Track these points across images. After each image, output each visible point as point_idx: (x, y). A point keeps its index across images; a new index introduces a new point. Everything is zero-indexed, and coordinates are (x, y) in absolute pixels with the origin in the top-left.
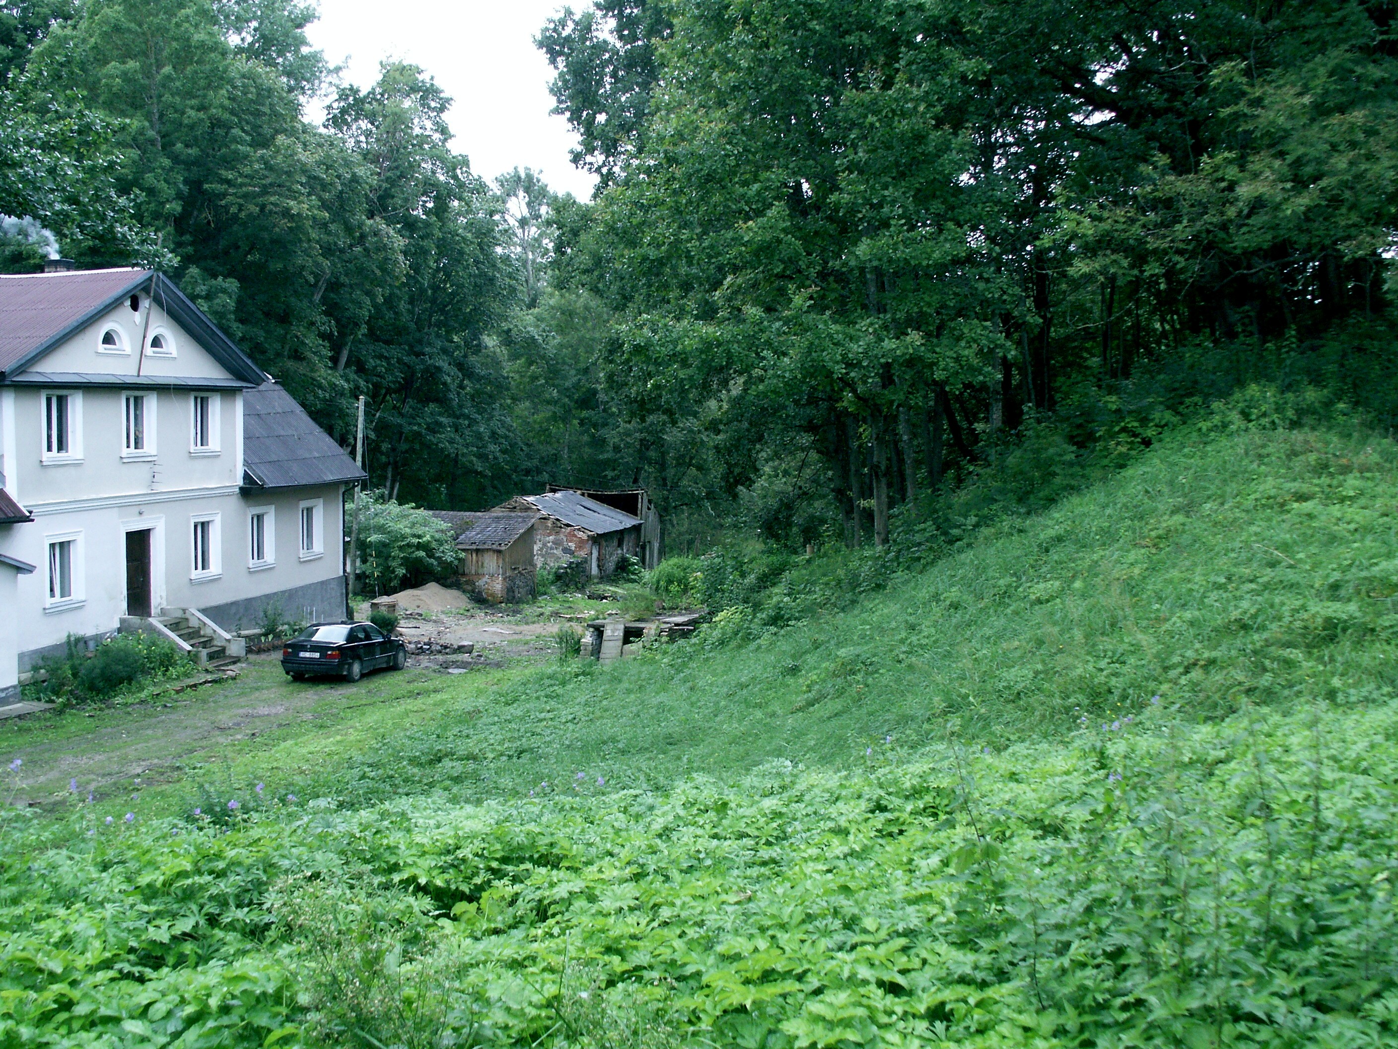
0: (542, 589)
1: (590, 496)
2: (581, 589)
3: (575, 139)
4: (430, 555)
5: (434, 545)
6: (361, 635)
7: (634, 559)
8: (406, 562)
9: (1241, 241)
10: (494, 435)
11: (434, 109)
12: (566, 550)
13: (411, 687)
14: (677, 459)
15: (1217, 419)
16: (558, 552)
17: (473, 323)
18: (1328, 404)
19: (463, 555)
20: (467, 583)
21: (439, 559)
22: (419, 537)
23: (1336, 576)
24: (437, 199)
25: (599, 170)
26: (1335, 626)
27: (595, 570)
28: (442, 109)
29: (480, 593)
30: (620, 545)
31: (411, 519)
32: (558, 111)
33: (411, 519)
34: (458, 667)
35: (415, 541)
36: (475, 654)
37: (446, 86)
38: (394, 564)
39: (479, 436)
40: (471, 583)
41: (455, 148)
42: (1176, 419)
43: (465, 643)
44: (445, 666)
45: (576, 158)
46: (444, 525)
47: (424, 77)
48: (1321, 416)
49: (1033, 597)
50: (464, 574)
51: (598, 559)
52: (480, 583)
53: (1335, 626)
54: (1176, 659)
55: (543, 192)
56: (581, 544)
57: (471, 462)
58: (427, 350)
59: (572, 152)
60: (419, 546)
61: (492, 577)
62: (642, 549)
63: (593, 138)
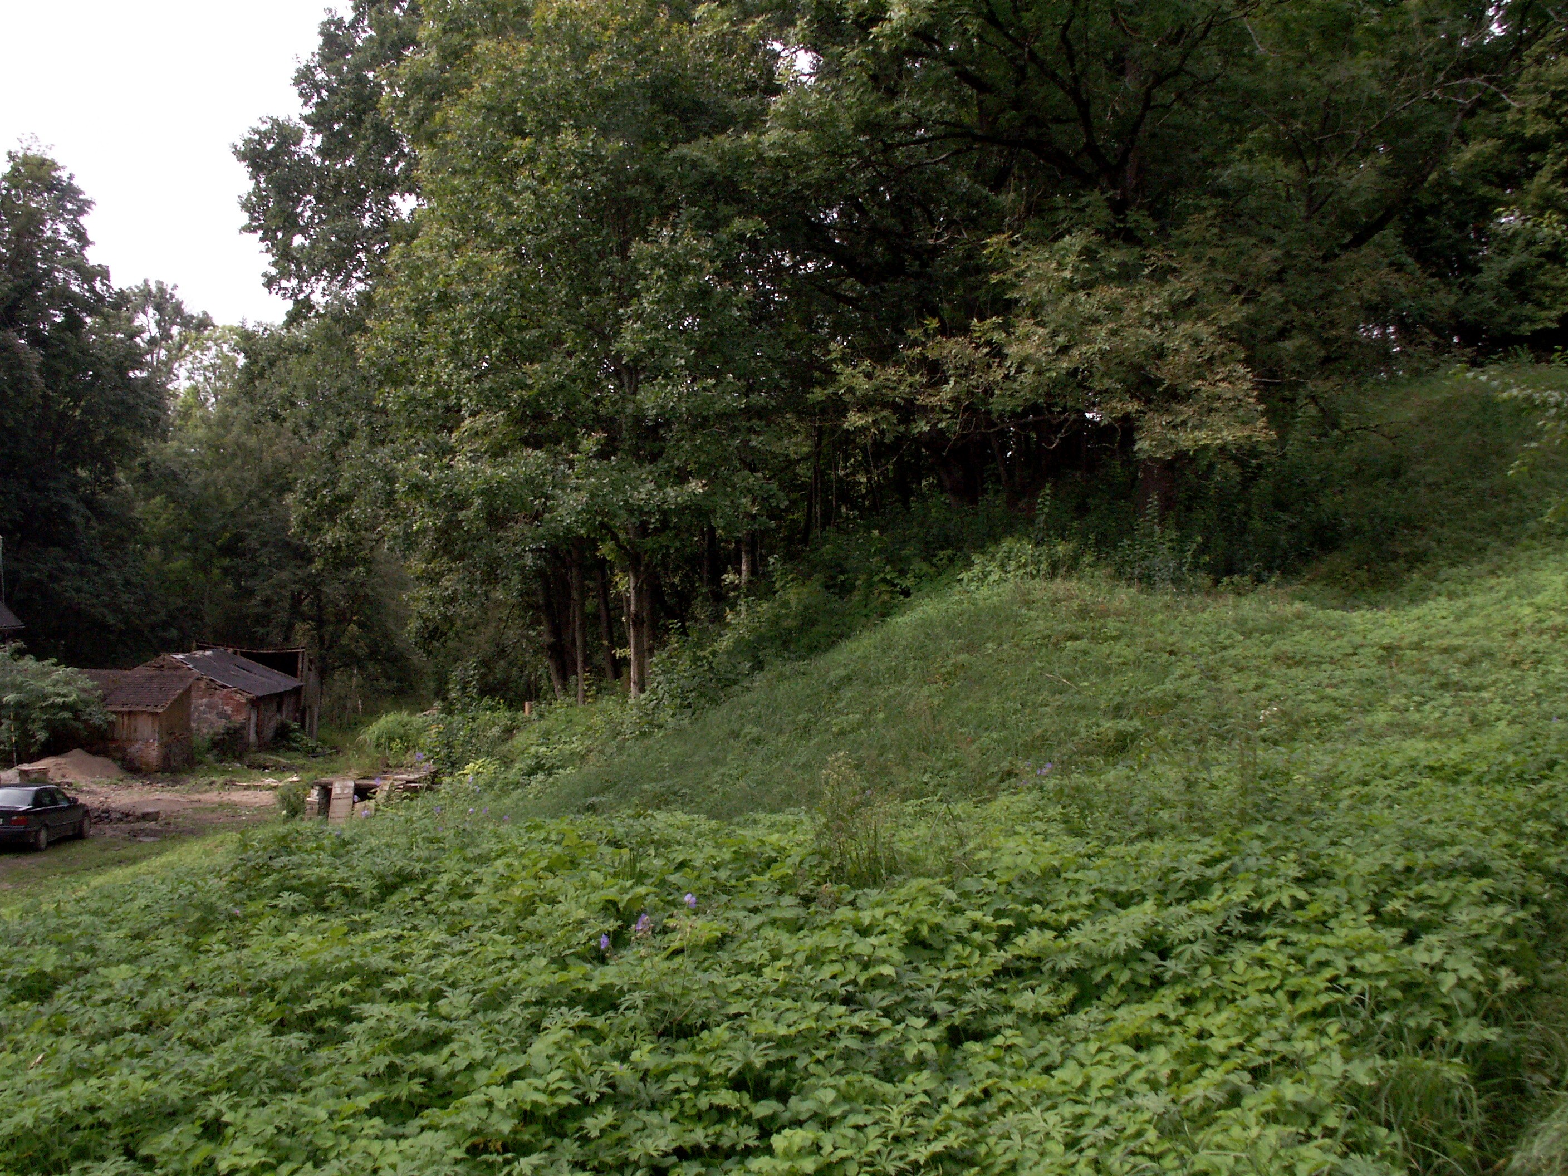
0: (198, 757)
1: (243, 654)
2: (239, 758)
3: (264, 262)
4: (76, 718)
5: (81, 706)
6: (47, 800)
7: (296, 725)
8: (49, 725)
9: (998, 404)
10: (127, 582)
11: (70, 212)
12: (222, 715)
13: (109, 854)
14: (336, 615)
15: (977, 569)
16: (212, 717)
17: (106, 455)
18: (1076, 558)
19: (113, 717)
20: (117, 749)
21: (85, 722)
22: (65, 696)
23: (1118, 699)
24: (69, 313)
25: (294, 295)
26: (1125, 737)
27: (253, 738)
28: (81, 212)
29: (132, 761)
30: (279, 709)
31: (54, 677)
32: (248, 229)
33: (54, 677)
34: (147, 835)
35: (60, 700)
36: (161, 821)
37: (86, 185)
38: (36, 726)
39: (111, 585)
40: (124, 750)
41: (93, 256)
42: (932, 570)
43: (150, 810)
44: (134, 835)
45: (270, 282)
46: (89, 684)
47: (64, 175)
48: (1072, 566)
49: (835, 729)
50: (113, 740)
51: (257, 725)
52: (133, 750)
53: (1125, 737)
54: (994, 769)
55: (178, 309)
56: (238, 708)
57: (102, 614)
58: (52, 484)
59: (265, 275)
60: (64, 707)
61: (148, 743)
62: (302, 714)
63: (285, 257)
